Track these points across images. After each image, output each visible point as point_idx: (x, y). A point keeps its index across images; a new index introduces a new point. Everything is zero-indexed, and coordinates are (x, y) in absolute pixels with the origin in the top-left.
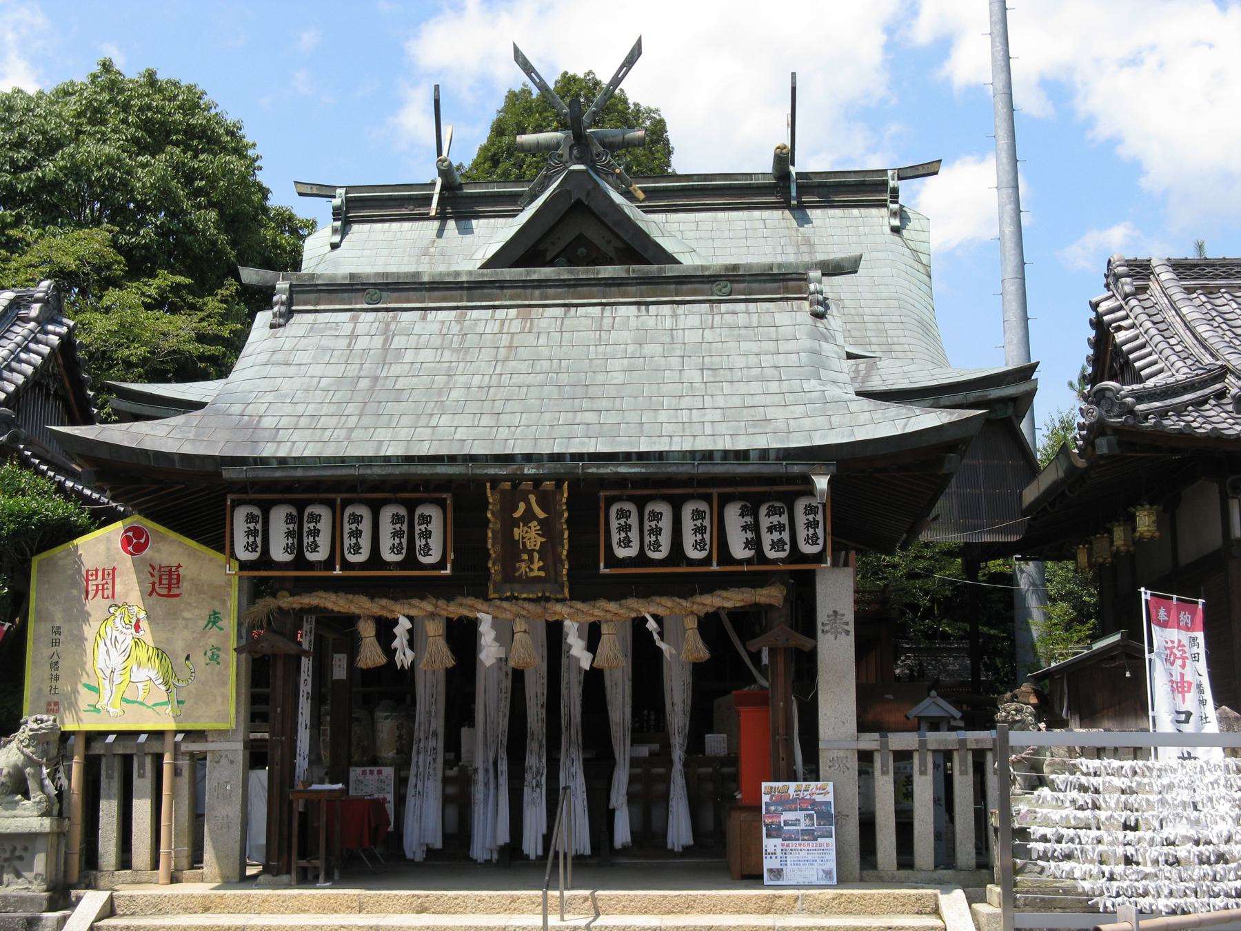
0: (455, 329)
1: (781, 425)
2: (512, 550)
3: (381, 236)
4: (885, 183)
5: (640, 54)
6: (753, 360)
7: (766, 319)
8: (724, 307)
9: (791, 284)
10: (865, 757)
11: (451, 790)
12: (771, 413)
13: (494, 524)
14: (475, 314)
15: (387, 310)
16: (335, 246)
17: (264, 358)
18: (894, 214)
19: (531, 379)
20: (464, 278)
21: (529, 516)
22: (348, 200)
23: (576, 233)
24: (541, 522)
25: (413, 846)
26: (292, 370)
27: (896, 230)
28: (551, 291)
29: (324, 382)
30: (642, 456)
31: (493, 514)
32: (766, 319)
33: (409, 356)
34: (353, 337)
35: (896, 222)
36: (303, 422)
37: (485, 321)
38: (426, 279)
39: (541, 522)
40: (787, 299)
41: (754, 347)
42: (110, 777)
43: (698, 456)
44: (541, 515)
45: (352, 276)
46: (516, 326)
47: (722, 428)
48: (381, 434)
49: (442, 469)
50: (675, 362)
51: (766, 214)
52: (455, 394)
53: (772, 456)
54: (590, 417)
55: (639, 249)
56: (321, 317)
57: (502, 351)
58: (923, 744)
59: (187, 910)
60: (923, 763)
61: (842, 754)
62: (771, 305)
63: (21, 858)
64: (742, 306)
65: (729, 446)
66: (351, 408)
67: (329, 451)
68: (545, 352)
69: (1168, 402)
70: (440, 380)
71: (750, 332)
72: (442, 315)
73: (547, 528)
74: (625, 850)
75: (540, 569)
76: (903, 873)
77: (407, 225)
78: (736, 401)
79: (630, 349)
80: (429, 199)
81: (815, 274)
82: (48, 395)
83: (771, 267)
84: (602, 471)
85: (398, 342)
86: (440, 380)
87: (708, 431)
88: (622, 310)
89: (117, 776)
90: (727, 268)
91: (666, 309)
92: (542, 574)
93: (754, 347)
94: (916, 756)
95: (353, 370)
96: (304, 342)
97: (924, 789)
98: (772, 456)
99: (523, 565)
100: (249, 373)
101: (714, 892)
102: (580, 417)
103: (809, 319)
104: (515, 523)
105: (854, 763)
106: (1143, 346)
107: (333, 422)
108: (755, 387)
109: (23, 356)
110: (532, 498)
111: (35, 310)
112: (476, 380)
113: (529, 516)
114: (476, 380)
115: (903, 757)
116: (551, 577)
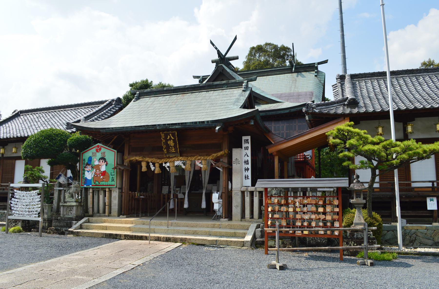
2: (168, 147)
18: (316, 72)
21: (170, 139)
22: (203, 79)
25: (183, 197)
27: (316, 76)
44: (173, 138)
53: (210, 122)
60: (256, 194)
73: (174, 141)
98: (210, 122)
104: (168, 140)
105: (240, 194)
110: (171, 135)
116: (176, 152)
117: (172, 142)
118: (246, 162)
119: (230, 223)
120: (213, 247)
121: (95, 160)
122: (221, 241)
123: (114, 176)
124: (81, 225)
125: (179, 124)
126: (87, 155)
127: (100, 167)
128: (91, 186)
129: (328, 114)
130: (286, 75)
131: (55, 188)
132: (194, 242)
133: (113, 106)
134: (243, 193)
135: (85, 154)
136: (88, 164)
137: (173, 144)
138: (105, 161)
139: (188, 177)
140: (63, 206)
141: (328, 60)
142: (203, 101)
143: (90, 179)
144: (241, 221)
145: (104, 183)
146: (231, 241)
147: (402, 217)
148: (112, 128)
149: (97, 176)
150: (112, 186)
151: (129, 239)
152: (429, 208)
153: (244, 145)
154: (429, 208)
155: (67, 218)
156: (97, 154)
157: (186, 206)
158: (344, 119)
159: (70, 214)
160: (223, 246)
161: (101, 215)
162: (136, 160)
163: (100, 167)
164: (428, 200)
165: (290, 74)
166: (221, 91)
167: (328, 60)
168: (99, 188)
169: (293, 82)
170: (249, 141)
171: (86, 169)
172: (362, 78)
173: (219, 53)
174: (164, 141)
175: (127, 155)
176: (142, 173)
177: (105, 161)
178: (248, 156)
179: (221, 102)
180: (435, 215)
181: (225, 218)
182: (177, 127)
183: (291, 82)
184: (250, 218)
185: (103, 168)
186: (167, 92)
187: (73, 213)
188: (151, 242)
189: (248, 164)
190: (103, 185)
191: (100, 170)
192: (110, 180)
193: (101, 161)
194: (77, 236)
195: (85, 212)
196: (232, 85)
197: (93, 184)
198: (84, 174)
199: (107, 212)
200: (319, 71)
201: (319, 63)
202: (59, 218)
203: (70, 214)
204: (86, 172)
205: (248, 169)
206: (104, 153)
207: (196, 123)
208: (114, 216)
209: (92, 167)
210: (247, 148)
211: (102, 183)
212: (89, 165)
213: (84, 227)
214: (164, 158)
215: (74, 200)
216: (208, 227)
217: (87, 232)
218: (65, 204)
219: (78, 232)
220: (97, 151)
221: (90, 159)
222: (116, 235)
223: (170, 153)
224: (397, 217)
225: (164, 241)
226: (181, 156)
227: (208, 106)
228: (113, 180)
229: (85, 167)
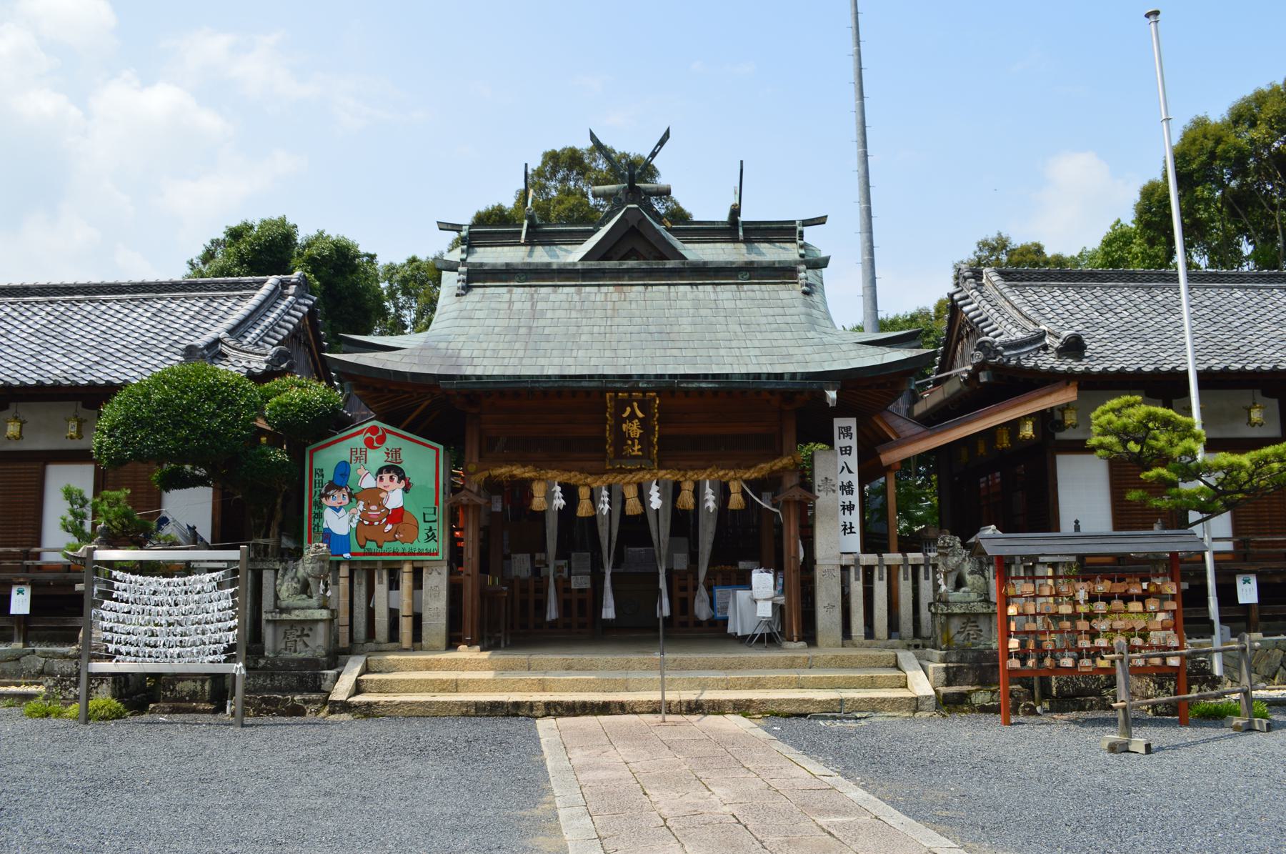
0: (576, 298)
1: (800, 358)
2: (621, 438)
4: (795, 229)
6: (771, 319)
7: (774, 295)
8: (745, 287)
12: (791, 351)
17: (455, 314)
18: (801, 247)
19: (630, 329)
22: (470, 233)
24: (640, 419)
26: (474, 322)
29: (497, 330)
30: (714, 376)
32: (774, 295)
33: (549, 314)
34: (510, 302)
35: (802, 251)
36: (488, 353)
37: (596, 295)
38: (555, 267)
39: (640, 419)
44: (640, 415)
45: (507, 264)
46: (615, 296)
47: (763, 360)
48: (542, 361)
49: (585, 384)
50: (721, 319)
51: (724, 245)
52: (584, 338)
53: (799, 377)
54: (676, 352)
56: (488, 290)
57: (609, 313)
58: (927, 560)
59: (416, 669)
63: (308, 635)
66: (517, 346)
67: (509, 372)
68: (637, 313)
70: (573, 329)
71: (765, 303)
72: (566, 290)
73: (644, 423)
74: (553, 624)
76: (868, 642)
77: (506, 249)
78: (767, 344)
79: (691, 311)
83: (774, 263)
85: (540, 306)
86: (573, 329)
87: (754, 361)
88: (681, 288)
90: (746, 263)
91: (710, 288)
93: (770, 311)
94: (876, 570)
95: (514, 323)
96: (479, 306)
97: (880, 589)
98: (799, 377)
100: (443, 325)
101: (711, 656)
102: (669, 352)
103: (802, 296)
104: (624, 420)
105: (838, 573)
106: (986, 319)
107: (508, 354)
108: (776, 335)
110: (635, 404)
111: (292, 289)
112: (596, 329)
113: (633, 416)
114: (596, 329)
115: (892, 571)
118: (847, 489)
119: (813, 652)
120: (834, 718)
121: (362, 472)
122: (854, 701)
123: (434, 526)
124: (358, 683)
126: (327, 459)
127: (383, 495)
128: (347, 555)
129: (1035, 371)
130: (718, 245)
132: (775, 709)
133: (290, 298)
134: (845, 568)
135: (320, 452)
136: (333, 486)
137: (639, 431)
138: (401, 476)
139: (607, 528)
140: (274, 622)
143: (345, 533)
145: (398, 546)
146: (884, 700)
147: (1222, 621)
149: (371, 523)
150: (428, 554)
151: (561, 715)
152: (1241, 600)
153: (839, 442)
154: (1241, 600)
155: (293, 660)
156: (371, 454)
157: (609, 612)
158: (1068, 384)
159: (300, 646)
160: (864, 715)
161: (384, 647)
162: (512, 476)
163: (383, 495)
164: (1239, 581)
165: (731, 245)
166: (734, 287)
168: (375, 562)
170: (854, 431)
171: (331, 502)
172: (1022, 280)
175: (475, 459)
177: (401, 476)
178: (850, 472)
180: (1255, 615)
181: (799, 640)
182: (704, 385)
184: (866, 638)
185: (395, 499)
187: (318, 643)
188: (669, 718)
189: (851, 492)
190: (395, 554)
191: (381, 506)
192: (422, 535)
193: (386, 477)
194: (367, 716)
195: (361, 638)
197: (355, 548)
198: (320, 516)
199: (406, 633)
201: (807, 223)
202: (262, 662)
203: (300, 646)
204: (328, 514)
205: (850, 507)
206: (397, 451)
207: (758, 376)
208: (434, 649)
209: (351, 496)
210: (846, 451)
211: (388, 547)
212: (339, 488)
214: (606, 472)
215: (314, 602)
216: (774, 667)
217: (406, 703)
218: (285, 616)
219: (369, 705)
220: (369, 443)
221: (343, 470)
222: (517, 705)
223: (625, 457)
224: (1212, 622)
225: (680, 713)
226: (661, 467)
228: (431, 537)
229: (321, 496)
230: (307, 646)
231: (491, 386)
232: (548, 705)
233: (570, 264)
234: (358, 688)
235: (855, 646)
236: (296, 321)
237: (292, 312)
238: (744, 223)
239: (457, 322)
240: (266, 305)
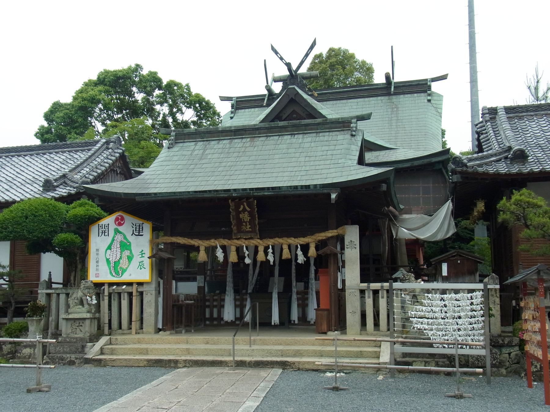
2: (240, 222)
3: (248, 113)
4: (427, 84)
5: (315, 44)
7: (335, 138)
8: (321, 134)
9: (345, 124)
10: (362, 292)
11: (238, 303)
13: (233, 213)
14: (236, 140)
15: (207, 141)
16: (232, 118)
20: (233, 129)
21: (244, 210)
22: (237, 102)
23: (292, 110)
24: (249, 212)
27: (429, 101)
28: (262, 131)
31: (232, 209)
40: (344, 130)
41: (327, 148)
42: (114, 300)
43: (292, 188)
49: (206, 195)
51: (383, 98)
53: (318, 187)
55: (313, 114)
61: (353, 291)
62: (338, 133)
63: (81, 326)
64: (328, 133)
65: (303, 184)
69: (483, 161)
72: (225, 142)
73: (251, 214)
75: (250, 228)
80: (264, 99)
81: (354, 121)
82: (117, 174)
84: (259, 194)
89: (116, 299)
91: (301, 136)
92: (250, 230)
94: (380, 292)
96: (177, 153)
97: (383, 303)
98: (318, 187)
99: (244, 227)
104: (240, 213)
105: (358, 294)
106: (489, 140)
109: (105, 161)
110: (245, 204)
113: (244, 210)
115: (376, 292)
117: (246, 216)
124: (102, 349)
125: (268, 188)
130: (379, 98)
131: (39, 291)
137: (249, 218)
140: (67, 319)
141: (447, 75)
142: (290, 151)
144: (361, 334)
148: (155, 194)
161: (125, 332)
165: (387, 98)
166: (315, 134)
167: (447, 75)
169: (392, 111)
173: (288, 65)
174: (234, 214)
176: (297, 264)
179: (321, 153)
182: (266, 194)
183: (389, 110)
186: (224, 134)
196: (333, 125)
200: (433, 93)
208: (149, 333)
213: (104, 351)
222: (170, 361)
223: (243, 232)
227: (302, 159)
230: (81, 331)
231: (159, 198)
232: (185, 361)
233: (228, 127)
234: (102, 352)
235: (368, 334)
236: (111, 162)
237: (109, 157)
238: (395, 83)
239: (165, 163)
240: (96, 154)
